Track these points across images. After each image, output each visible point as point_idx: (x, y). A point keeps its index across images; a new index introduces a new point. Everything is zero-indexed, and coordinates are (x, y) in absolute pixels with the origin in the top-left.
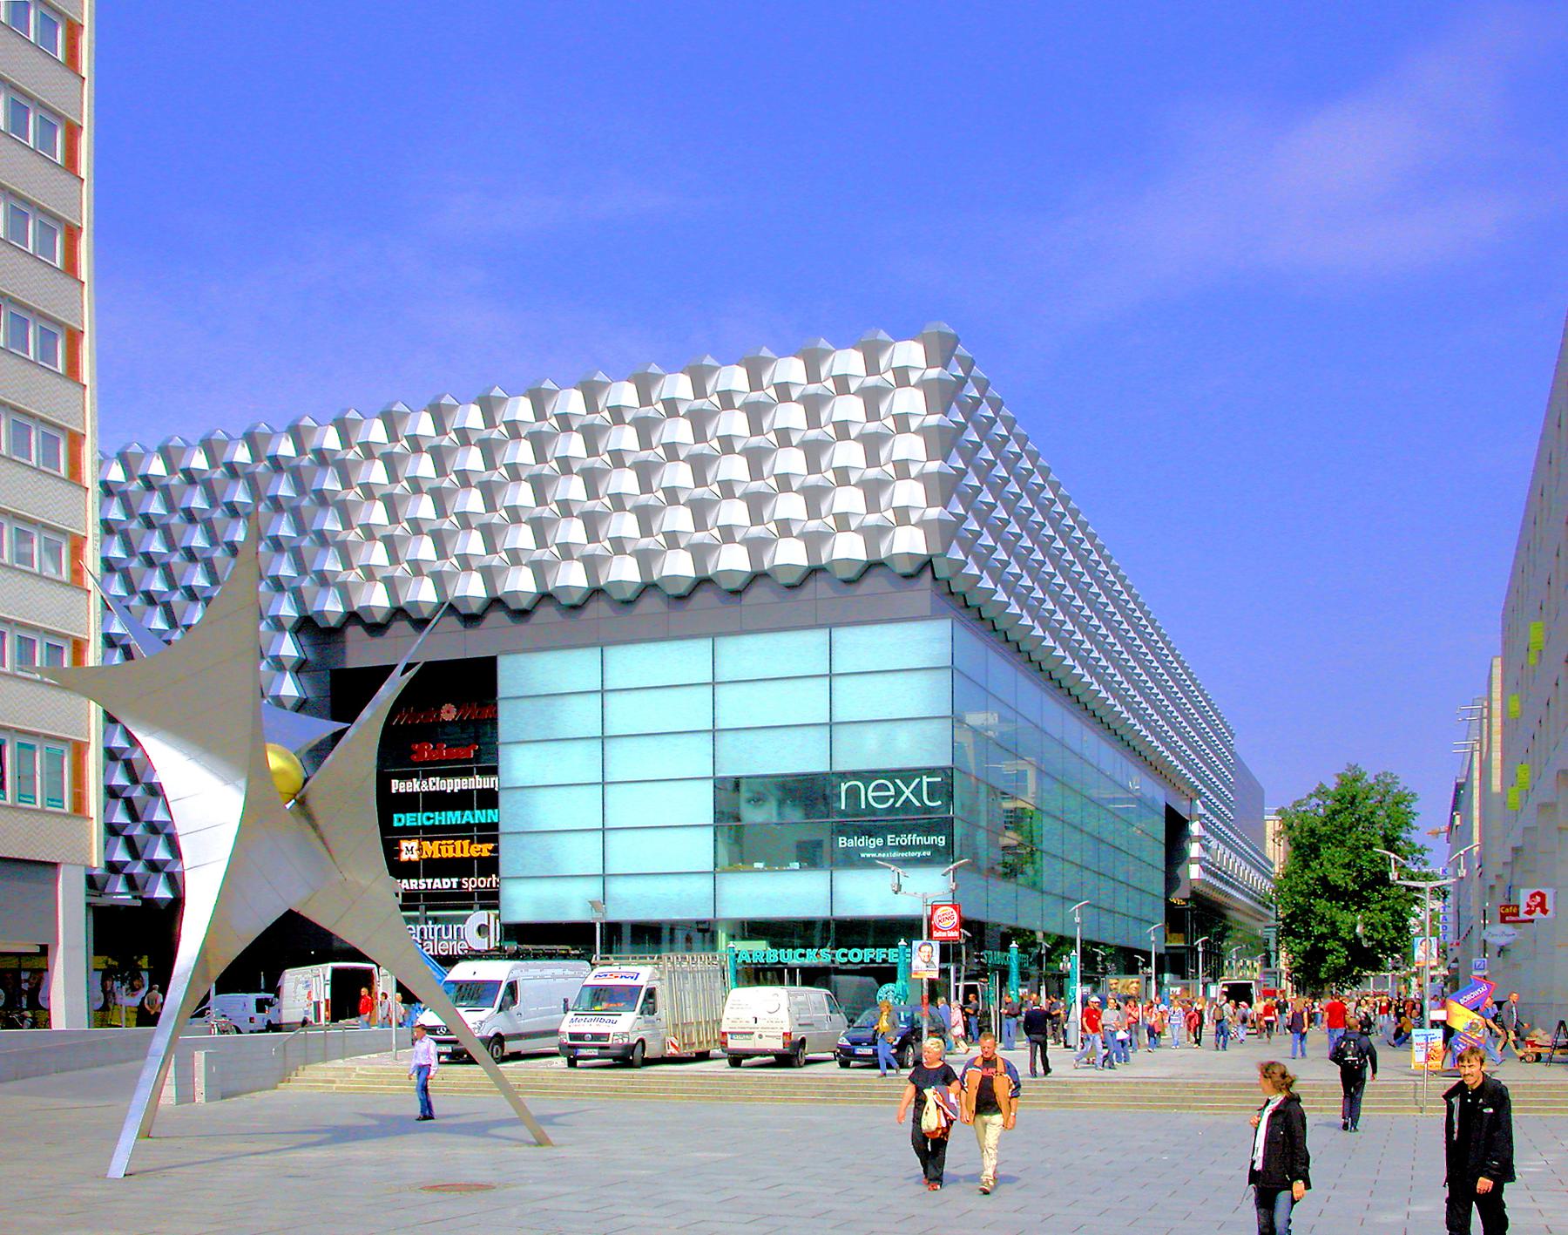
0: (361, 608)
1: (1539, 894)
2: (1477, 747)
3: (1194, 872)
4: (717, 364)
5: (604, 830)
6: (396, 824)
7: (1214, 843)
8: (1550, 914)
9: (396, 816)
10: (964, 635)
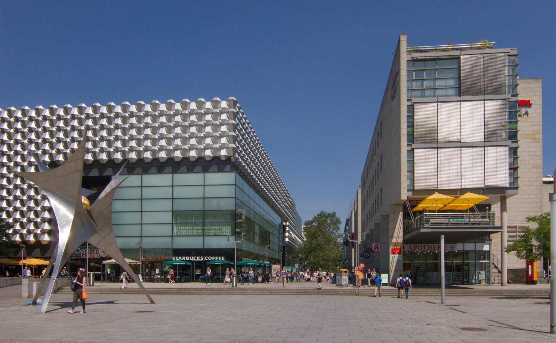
0: (56, 160)
1: (377, 245)
2: (353, 210)
3: (287, 240)
4: (130, 104)
7: (291, 232)
8: (379, 250)
10: (238, 177)
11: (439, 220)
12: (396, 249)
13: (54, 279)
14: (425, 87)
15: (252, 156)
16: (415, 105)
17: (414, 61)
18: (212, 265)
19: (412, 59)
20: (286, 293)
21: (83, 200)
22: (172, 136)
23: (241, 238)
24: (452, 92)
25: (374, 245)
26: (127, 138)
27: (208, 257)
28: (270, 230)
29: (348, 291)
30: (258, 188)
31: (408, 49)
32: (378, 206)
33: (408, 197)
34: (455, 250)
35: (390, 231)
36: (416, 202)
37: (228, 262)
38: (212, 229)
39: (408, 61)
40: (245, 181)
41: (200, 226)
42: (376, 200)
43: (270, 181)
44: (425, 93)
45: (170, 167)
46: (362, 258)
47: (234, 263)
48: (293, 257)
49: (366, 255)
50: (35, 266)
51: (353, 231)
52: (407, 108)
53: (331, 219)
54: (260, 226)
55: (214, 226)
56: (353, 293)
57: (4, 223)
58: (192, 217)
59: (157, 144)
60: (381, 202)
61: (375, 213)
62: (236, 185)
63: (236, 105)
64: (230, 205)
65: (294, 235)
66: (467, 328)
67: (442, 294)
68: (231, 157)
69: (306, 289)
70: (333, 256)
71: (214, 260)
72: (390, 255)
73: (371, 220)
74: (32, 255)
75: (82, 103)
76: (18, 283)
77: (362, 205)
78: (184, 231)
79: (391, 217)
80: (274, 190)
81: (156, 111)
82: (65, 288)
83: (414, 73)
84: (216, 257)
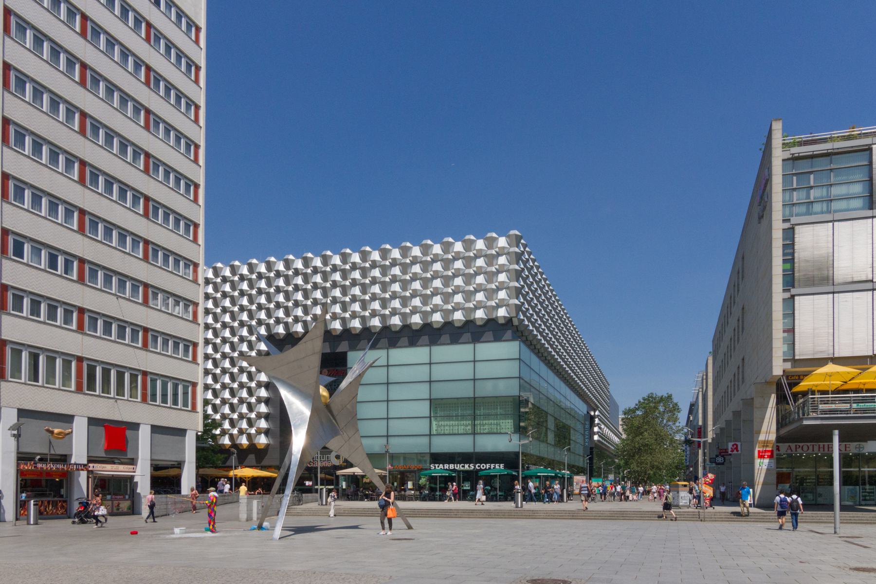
2: (701, 390)
3: (596, 438)
5: (388, 419)
7: (603, 426)
8: (739, 452)
10: (523, 346)
11: (833, 406)
12: (765, 450)
13: (288, 496)
14: (812, 199)
15: (540, 310)
16: (797, 228)
17: (795, 159)
18: (485, 476)
19: (791, 156)
20: (595, 516)
21: (321, 391)
22: (429, 292)
23: (529, 436)
24: (858, 203)
25: (730, 445)
26: (367, 297)
27: (481, 464)
28: (570, 422)
29: (688, 515)
30: (549, 358)
31: (786, 142)
32: (738, 385)
33: (784, 371)
34: (864, 451)
35: (755, 423)
36: (797, 378)
37: (510, 471)
38: (485, 425)
39: (783, 160)
40: (533, 352)
41: (469, 420)
42: (735, 375)
43: (570, 350)
44: (812, 207)
45: (427, 337)
46: (714, 465)
47: (518, 474)
48: (605, 464)
49: (720, 460)
50: (249, 478)
51: (700, 423)
52: (783, 233)
53: (664, 406)
54: (556, 419)
55: (489, 420)
56: (696, 518)
57: (210, 421)
58: (458, 407)
59: (408, 305)
60: (743, 378)
61: (734, 395)
62: (520, 359)
63: (519, 242)
64: (511, 389)
65: (606, 431)
66: (862, 568)
67: (835, 520)
68: (513, 319)
69: (624, 511)
70: (667, 461)
71: (490, 468)
72: (756, 460)
73: (728, 406)
74: (245, 463)
75: (308, 252)
76: (235, 500)
77: (714, 382)
78: (446, 428)
79: (757, 402)
80: (576, 364)
81: (407, 258)
82: (292, 508)
83: (795, 178)
84: (492, 465)
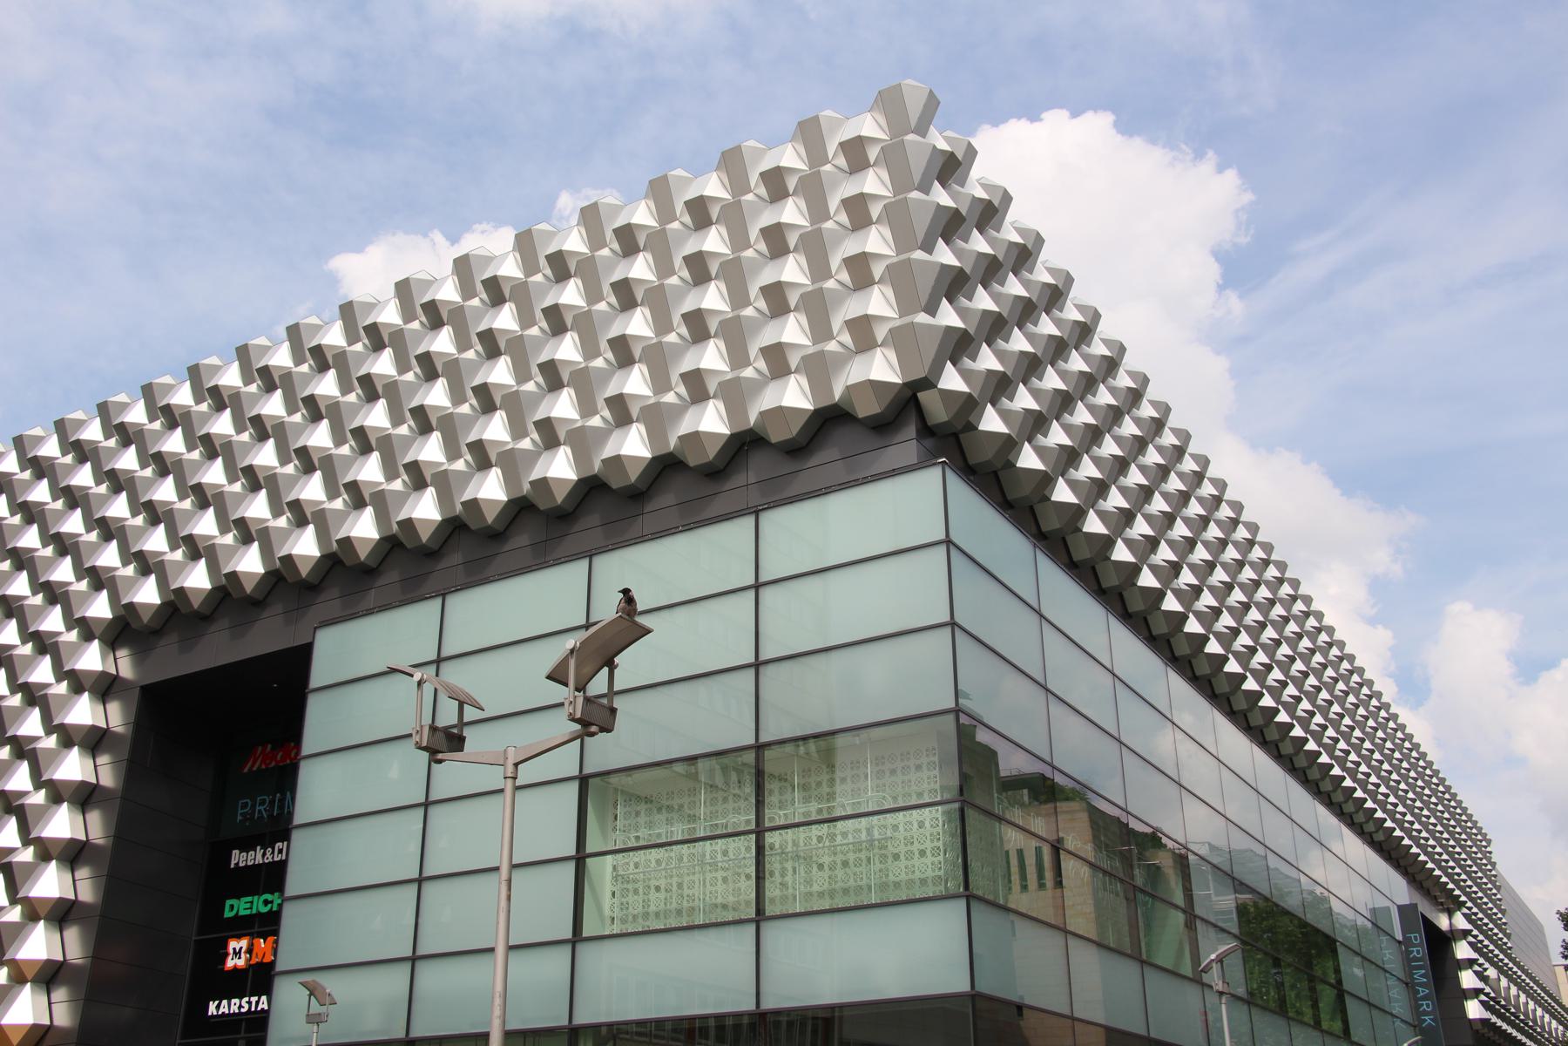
6: (228, 914)
7: (1492, 973)
9: (229, 902)
